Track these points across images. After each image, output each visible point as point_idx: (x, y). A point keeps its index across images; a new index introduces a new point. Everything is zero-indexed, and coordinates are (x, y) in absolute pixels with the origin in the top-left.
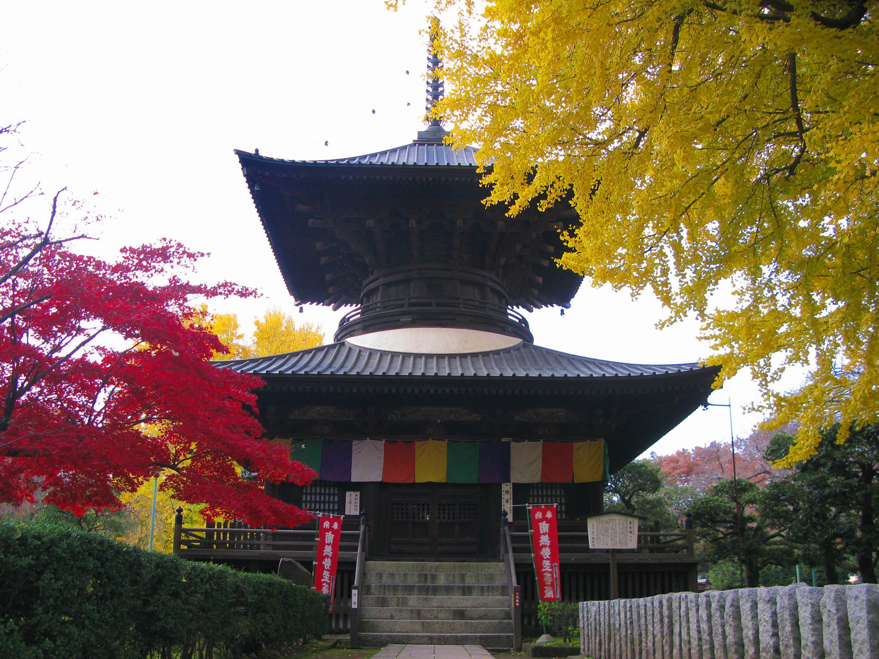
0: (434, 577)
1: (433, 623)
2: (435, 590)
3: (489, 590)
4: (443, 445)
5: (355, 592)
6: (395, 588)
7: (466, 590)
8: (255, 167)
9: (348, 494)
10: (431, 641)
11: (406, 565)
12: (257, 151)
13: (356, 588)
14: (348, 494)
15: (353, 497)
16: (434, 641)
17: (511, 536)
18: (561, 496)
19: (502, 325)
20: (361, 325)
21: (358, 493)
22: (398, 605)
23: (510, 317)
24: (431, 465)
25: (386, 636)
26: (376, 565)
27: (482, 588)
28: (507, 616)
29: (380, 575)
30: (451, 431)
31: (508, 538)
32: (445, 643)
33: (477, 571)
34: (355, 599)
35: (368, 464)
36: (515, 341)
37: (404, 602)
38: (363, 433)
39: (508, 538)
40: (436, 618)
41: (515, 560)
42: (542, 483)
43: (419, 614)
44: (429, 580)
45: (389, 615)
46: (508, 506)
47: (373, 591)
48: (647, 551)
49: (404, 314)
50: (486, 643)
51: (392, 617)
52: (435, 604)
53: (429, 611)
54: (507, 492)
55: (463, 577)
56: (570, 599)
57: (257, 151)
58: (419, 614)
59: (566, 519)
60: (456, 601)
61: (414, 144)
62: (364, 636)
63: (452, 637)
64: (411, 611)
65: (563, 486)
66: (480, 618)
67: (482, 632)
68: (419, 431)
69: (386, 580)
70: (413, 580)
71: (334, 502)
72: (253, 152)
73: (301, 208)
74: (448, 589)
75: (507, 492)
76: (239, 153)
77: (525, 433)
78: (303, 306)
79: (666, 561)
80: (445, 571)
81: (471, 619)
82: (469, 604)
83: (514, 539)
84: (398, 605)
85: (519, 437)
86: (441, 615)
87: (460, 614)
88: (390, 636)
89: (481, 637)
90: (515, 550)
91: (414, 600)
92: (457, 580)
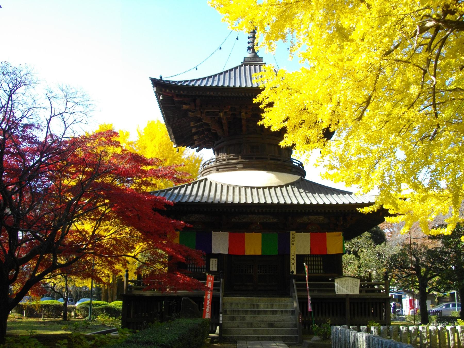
0: (258, 305)
1: (259, 330)
2: (259, 312)
3: (284, 309)
4: (259, 235)
5: (221, 315)
6: (239, 311)
7: (274, 312)
8: (160, 85)
9: (211, 260)
10: (258, 339)
11: (243, 299)
12: (161, 77)
13: (221, 313)
14: (211, 260)
15: (214, 262)
16: (259, 339)
17: (296, 284)
18: (320, 261)
19: (290, 168)
20: (215, 168)
21: (217, 259)
22: (241, 320)
23: (294, 163)
24: (254, 245)
25: (236, 337)
26: (226, 298)
27: (282, 311)
28: (295, 326)
29: (231, 304)
30: (264, 228)
31: (295, 286)
32: (265, 340)
33: (279, 303)
34: (221, 319)
35: (221, 243)
36: (296, 178)
37: (244, 319)
38: (219, 229)
39: (295, 286)
40: (260, 327)
41: (298, 296)
42: (311, 255)
43: (251, 325)
44: (269, 307)
45: (236, 325)
46: (293, 268)
47: (228, 313)
48: (364, 291)
49: (239, 163)
50: (284, 340)
51: (238, 327)
52: (259, 320)
53: (256, 323)
54: (293, 259)
55: (272, 305)
56: (325, 315)
57: (161, 77)
58: (251, 325)
59: (323, 273)
60: (270, 318)
61: (244, 65)
62: (226, 336)
63: (269, 337)
64: (248, 324)
65: (322, 256)
66: (280, 327)
67: (283, 334)
68: (248, 227)
69: (234, 308)
70: (247, 308)
71: (321, 269)
72: (159, 78)
73: (185, 107)
74: (265, 312)
75: (293, 259)
76: (160, 85)
77: (301, 229)
78: (179, 148)
79: (374, 297)
80: (263, 303)
81: (277, 327)
82: (276, 319)
83: (298, 285)
84: (241, 320)
85: (299, 230)
86: (262, 325)
87: (271, 325)
88: (238, 337)
89: (282, 337)
90: (298, 291)
91: (248, 318)
92: (269, 307)
